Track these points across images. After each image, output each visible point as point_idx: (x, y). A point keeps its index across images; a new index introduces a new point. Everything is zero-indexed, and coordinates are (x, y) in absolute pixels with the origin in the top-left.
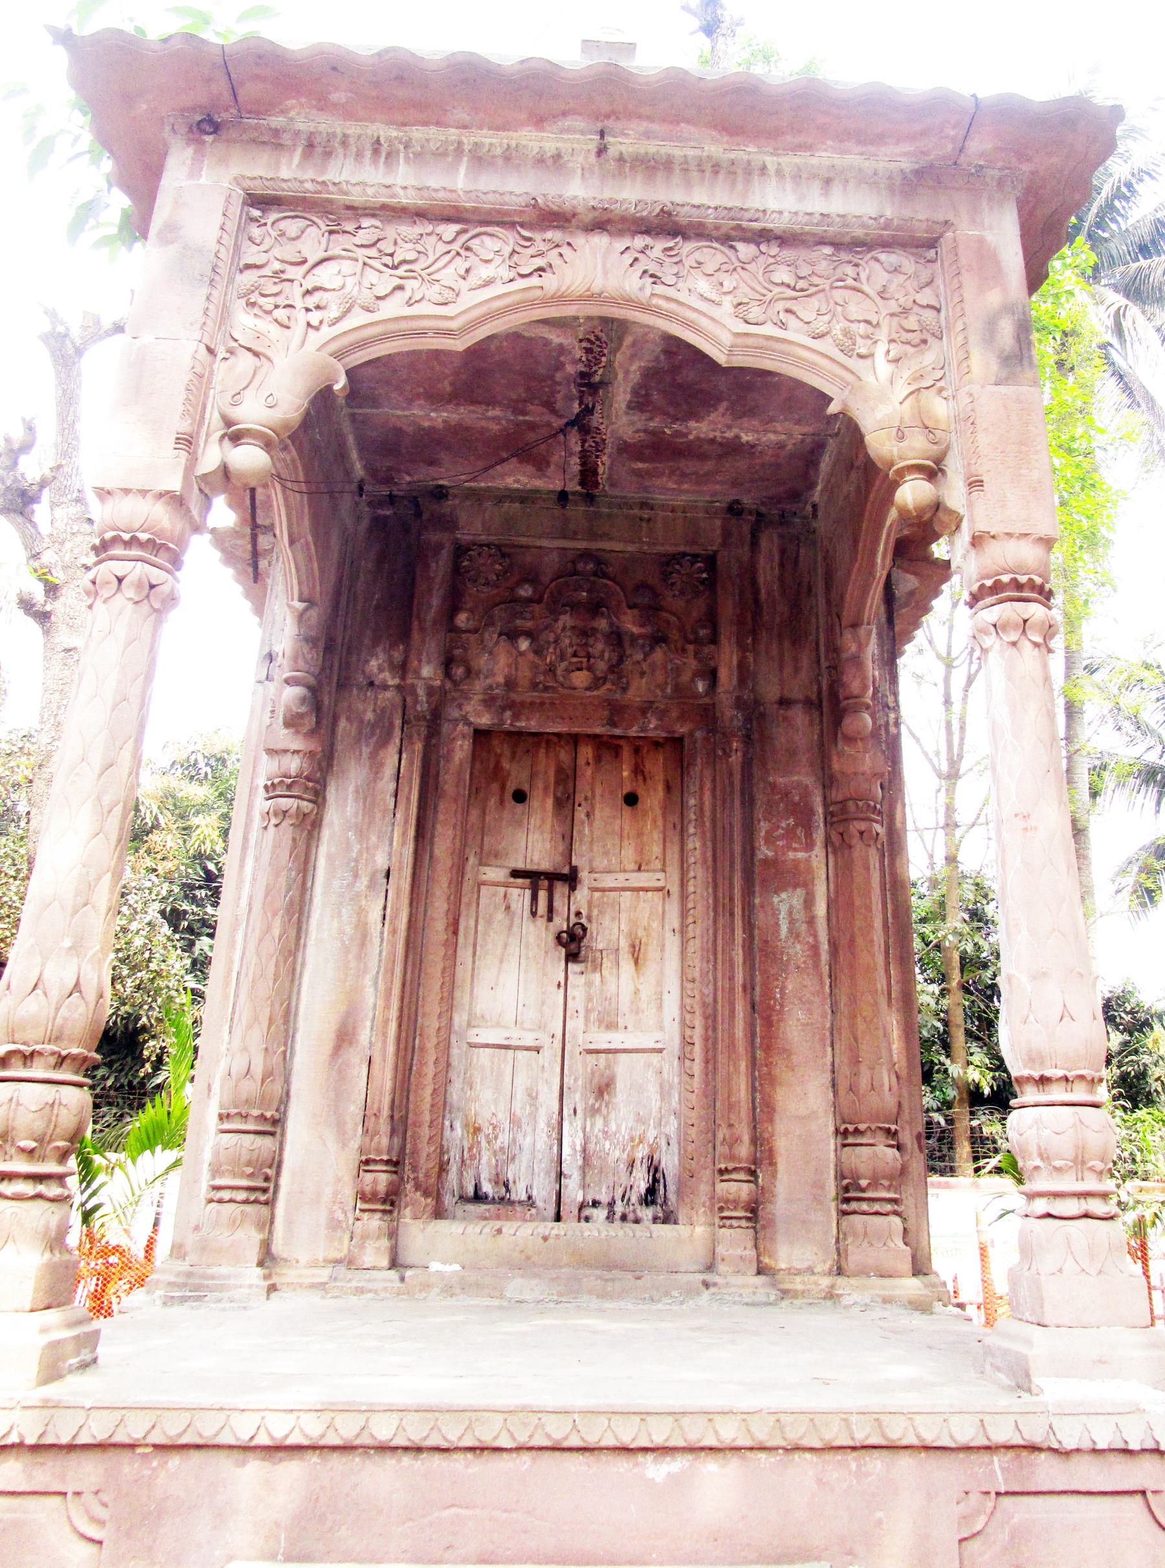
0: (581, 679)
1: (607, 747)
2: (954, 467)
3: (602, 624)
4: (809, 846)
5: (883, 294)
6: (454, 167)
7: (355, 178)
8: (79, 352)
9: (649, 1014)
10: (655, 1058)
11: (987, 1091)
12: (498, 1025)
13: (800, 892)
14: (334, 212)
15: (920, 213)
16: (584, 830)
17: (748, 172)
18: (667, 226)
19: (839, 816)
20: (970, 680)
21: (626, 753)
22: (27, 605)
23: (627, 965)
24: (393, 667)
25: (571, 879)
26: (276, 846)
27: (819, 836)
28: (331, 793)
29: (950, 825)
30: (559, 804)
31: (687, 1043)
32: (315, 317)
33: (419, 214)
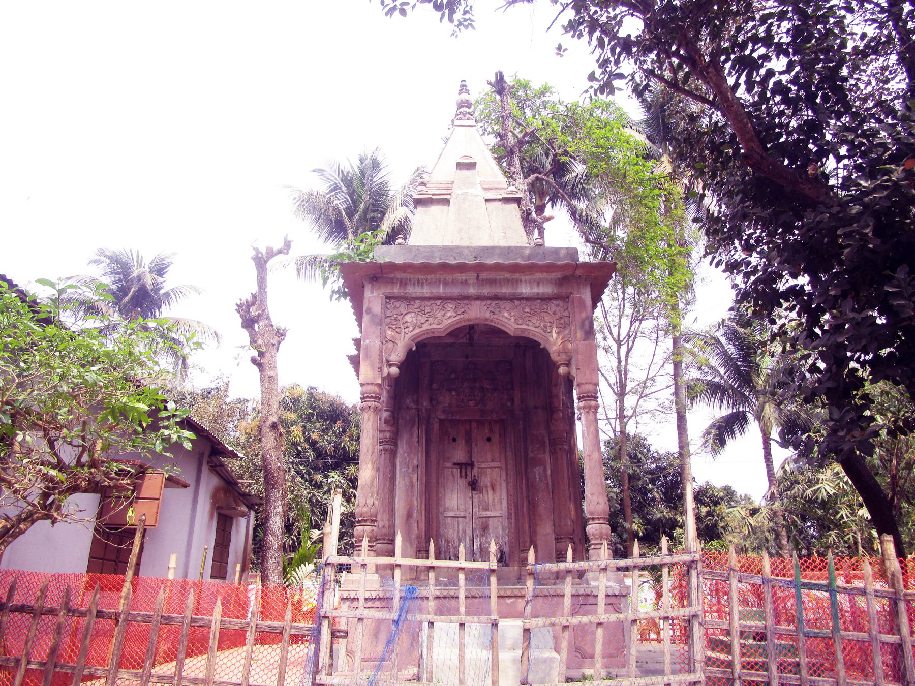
0: (472, 403)
1: (480, 423)
2: (573, 362)
3: (477, 385)
4: (545, 453)
7: (413, 290)
8: (266, 262)
9: (498, 507)
10: (500, 519)
11: (641, 534)
12: (453, 510)
15: (564, 291)
18: (496, 298)
19: (553, 443)
20: (629, 351)
22: (254, 361)
23: (490, 492)
25: (472, 465)
26: (385, 460)
27: (547, 449)
28: (399, 443)
29: (621, 416)
30: (466, 441)
31: (509, 514)
32: (406, 330)
33: (430, 299)
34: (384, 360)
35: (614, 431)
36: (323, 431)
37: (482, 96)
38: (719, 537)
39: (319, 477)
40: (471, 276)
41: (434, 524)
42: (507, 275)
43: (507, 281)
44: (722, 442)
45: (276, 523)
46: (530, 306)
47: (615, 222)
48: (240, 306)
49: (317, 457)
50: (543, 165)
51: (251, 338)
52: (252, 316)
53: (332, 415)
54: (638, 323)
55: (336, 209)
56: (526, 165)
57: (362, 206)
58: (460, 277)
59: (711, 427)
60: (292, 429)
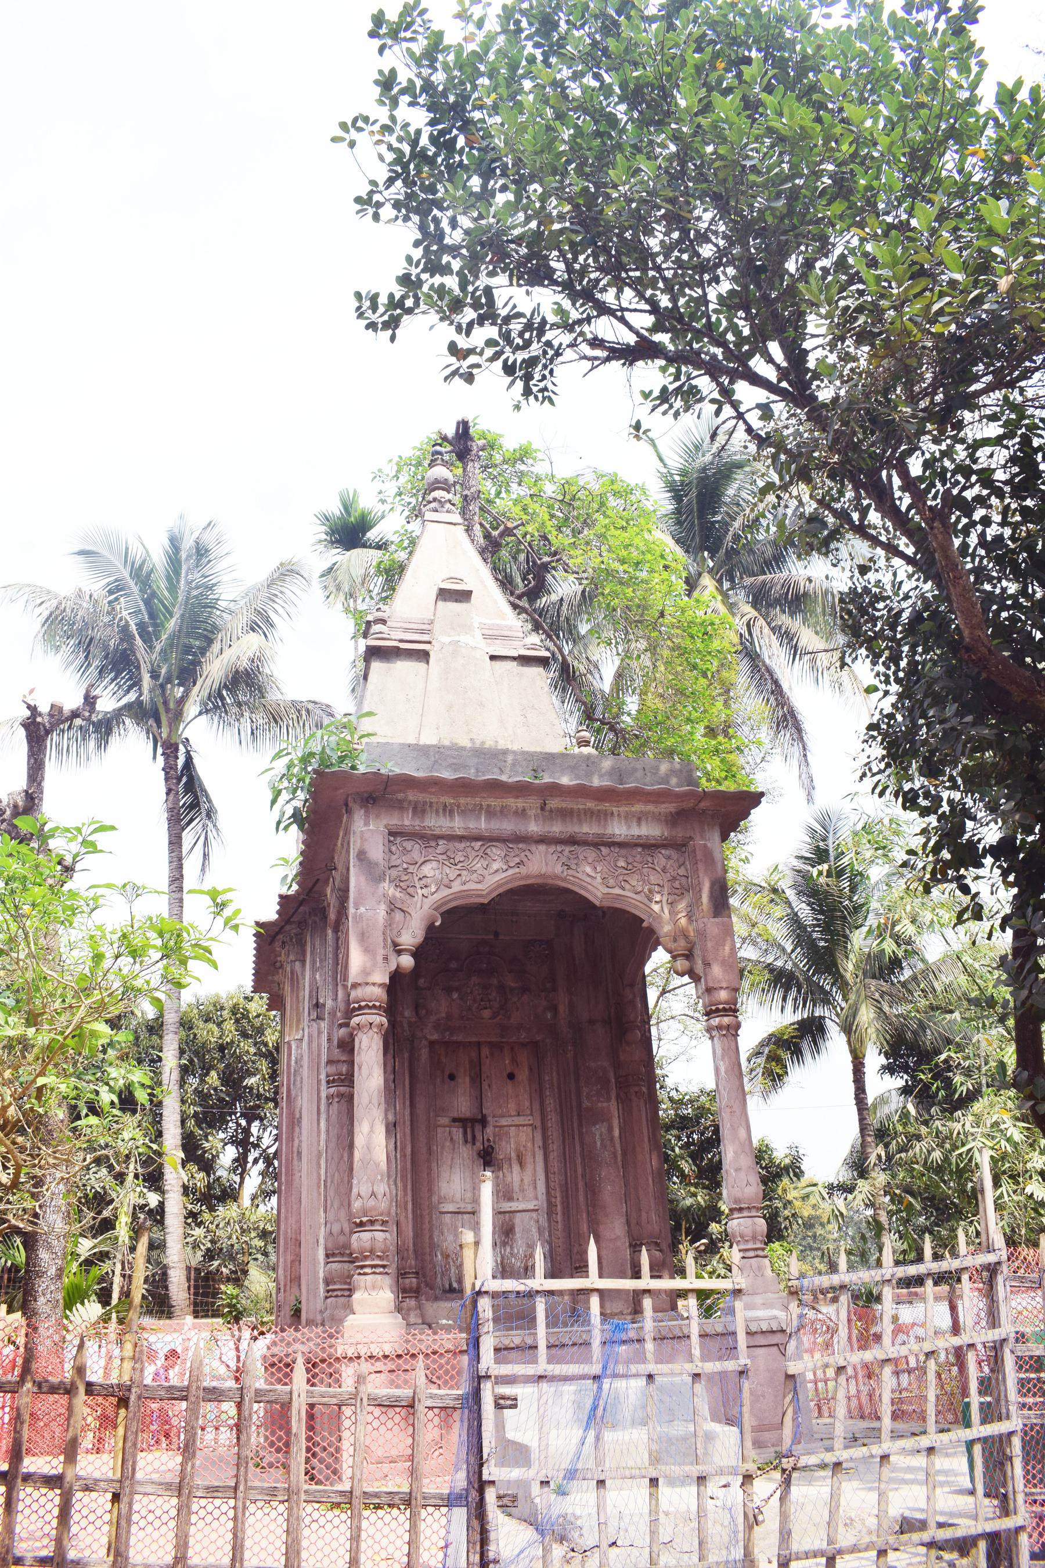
0: (487, 1013)
1: (497, 1047)
2: (697, 952)
3: (495, 981)
4: (609, 1100)
5: (664, 870)
6: (479, 818)
7: (437, 823)
14: (427, 838)
15: (680, 833)
16: (488, 1094)
18: (572, 841)
23: (516, 1168)
25: (483, 1121)
27: (613, 1094)
30: (473, 1080)
31: (551, 1205)
32: (425, 891)
33: (461, 838)
40: (531, 803)
42: (590, 804)
43: (590, 814)
58: (513, 803)
59: (762, 1044)
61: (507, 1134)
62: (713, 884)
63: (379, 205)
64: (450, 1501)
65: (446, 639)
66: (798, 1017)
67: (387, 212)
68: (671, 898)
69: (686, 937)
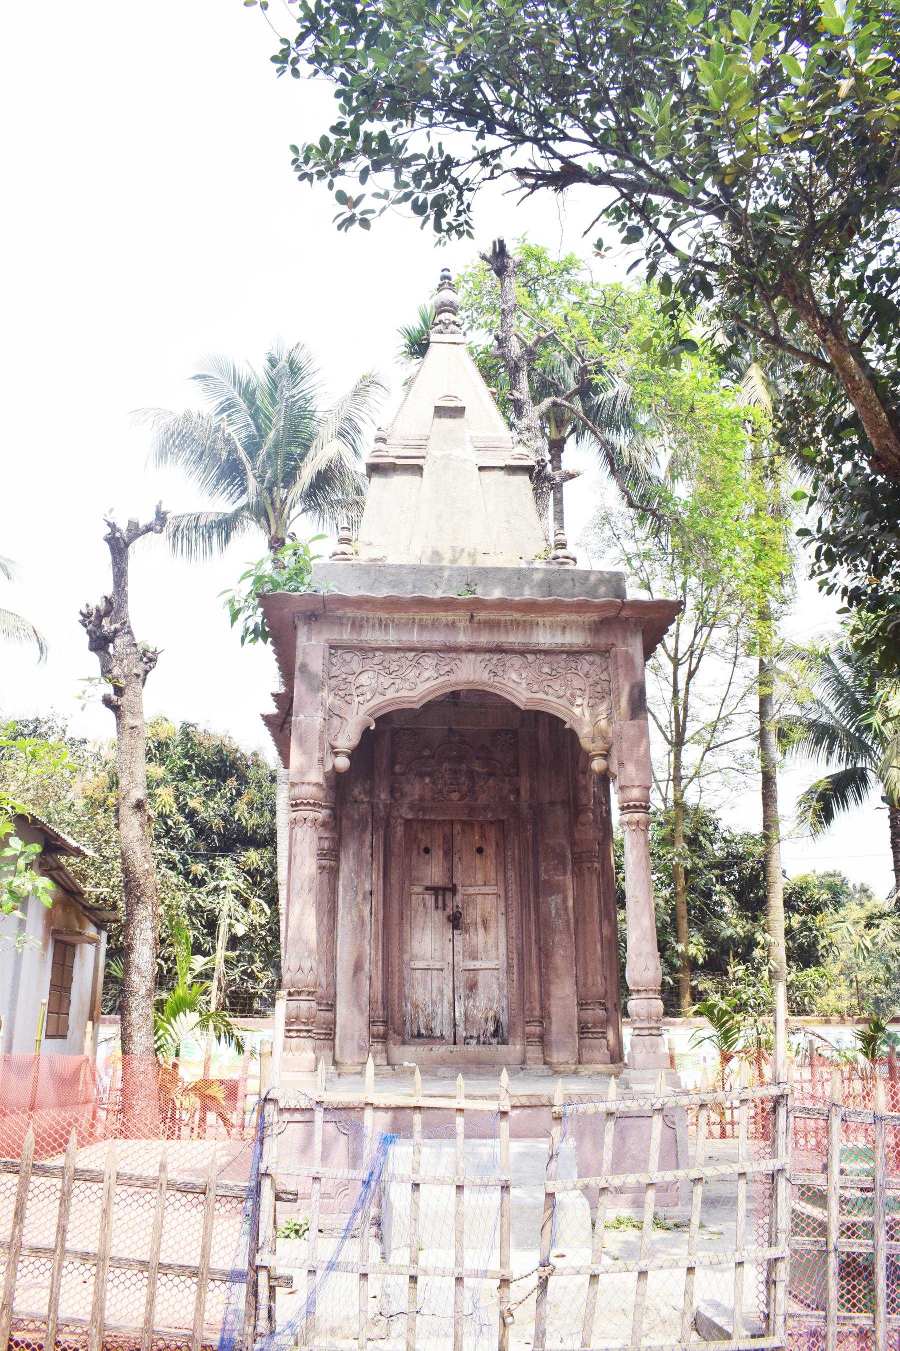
0: (455, 796)
1: (467, 825)
2: (614, 751)
3: (464, 767)
4: (565, 873)
6: (412, 630)
7: (373, 637)
8: (127, 545)
9: (493, 954)
11: (701, 961)
13: (560, 896)
14: (365, 651)
15: (602, 641)
17: (531, 625)
18: (499, 650)
20: (691, 675)
21: (477, 828)
22: (107, 702)
23: (481, 931)
24: (365, 793)
25: (453, 890)
27: (569, 868)
28: (342, 857)
29: (677, 779)
30: (445, 854)
31: (510, 966)
32: (361, 699)
33: (397, 649)
34: (327, 745)
35: (665, 800)
36: (207, 794)
37: (469, 270)
38: (817, 963)
39: (199, 868)
40: (461, 617)
41: (396, 981)
42: (517, 616)
43: (517, 624)
44: (826, 815)
45: (143, 957)
46: (550, 663)
47: (675, 469)
48: (86, 616)
49: (197, 836)
50: (562, 379)
51: (103, 666)
52: (104, 629)
53: (221, 767)
54: (706, 630)
55: (228, 441)
56: (535, 378)
57: (272, 435)
60: (158, 791)
61: (474, 901)
62: (632, 688)
63: (295, 61)
64: (234, 1277)
65: (438, 454)
66: (842, 768)
67: (305, 68)
68: (592, 702)
69: (604, 738)
